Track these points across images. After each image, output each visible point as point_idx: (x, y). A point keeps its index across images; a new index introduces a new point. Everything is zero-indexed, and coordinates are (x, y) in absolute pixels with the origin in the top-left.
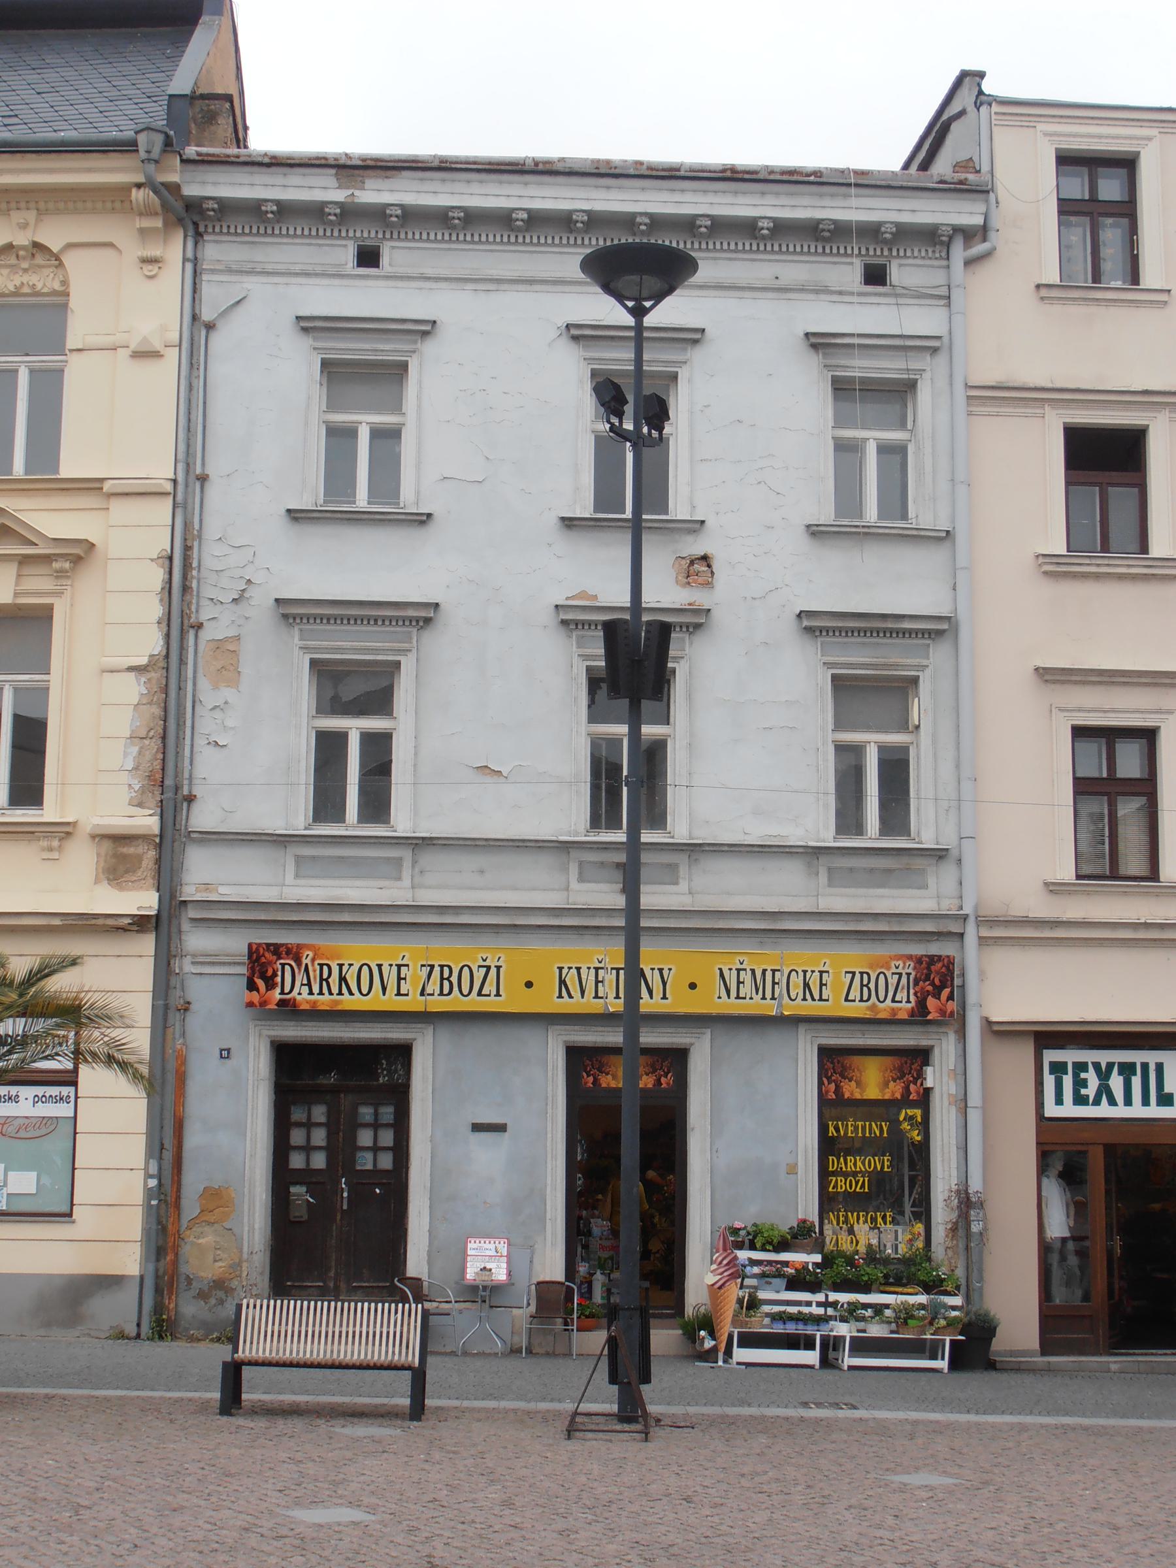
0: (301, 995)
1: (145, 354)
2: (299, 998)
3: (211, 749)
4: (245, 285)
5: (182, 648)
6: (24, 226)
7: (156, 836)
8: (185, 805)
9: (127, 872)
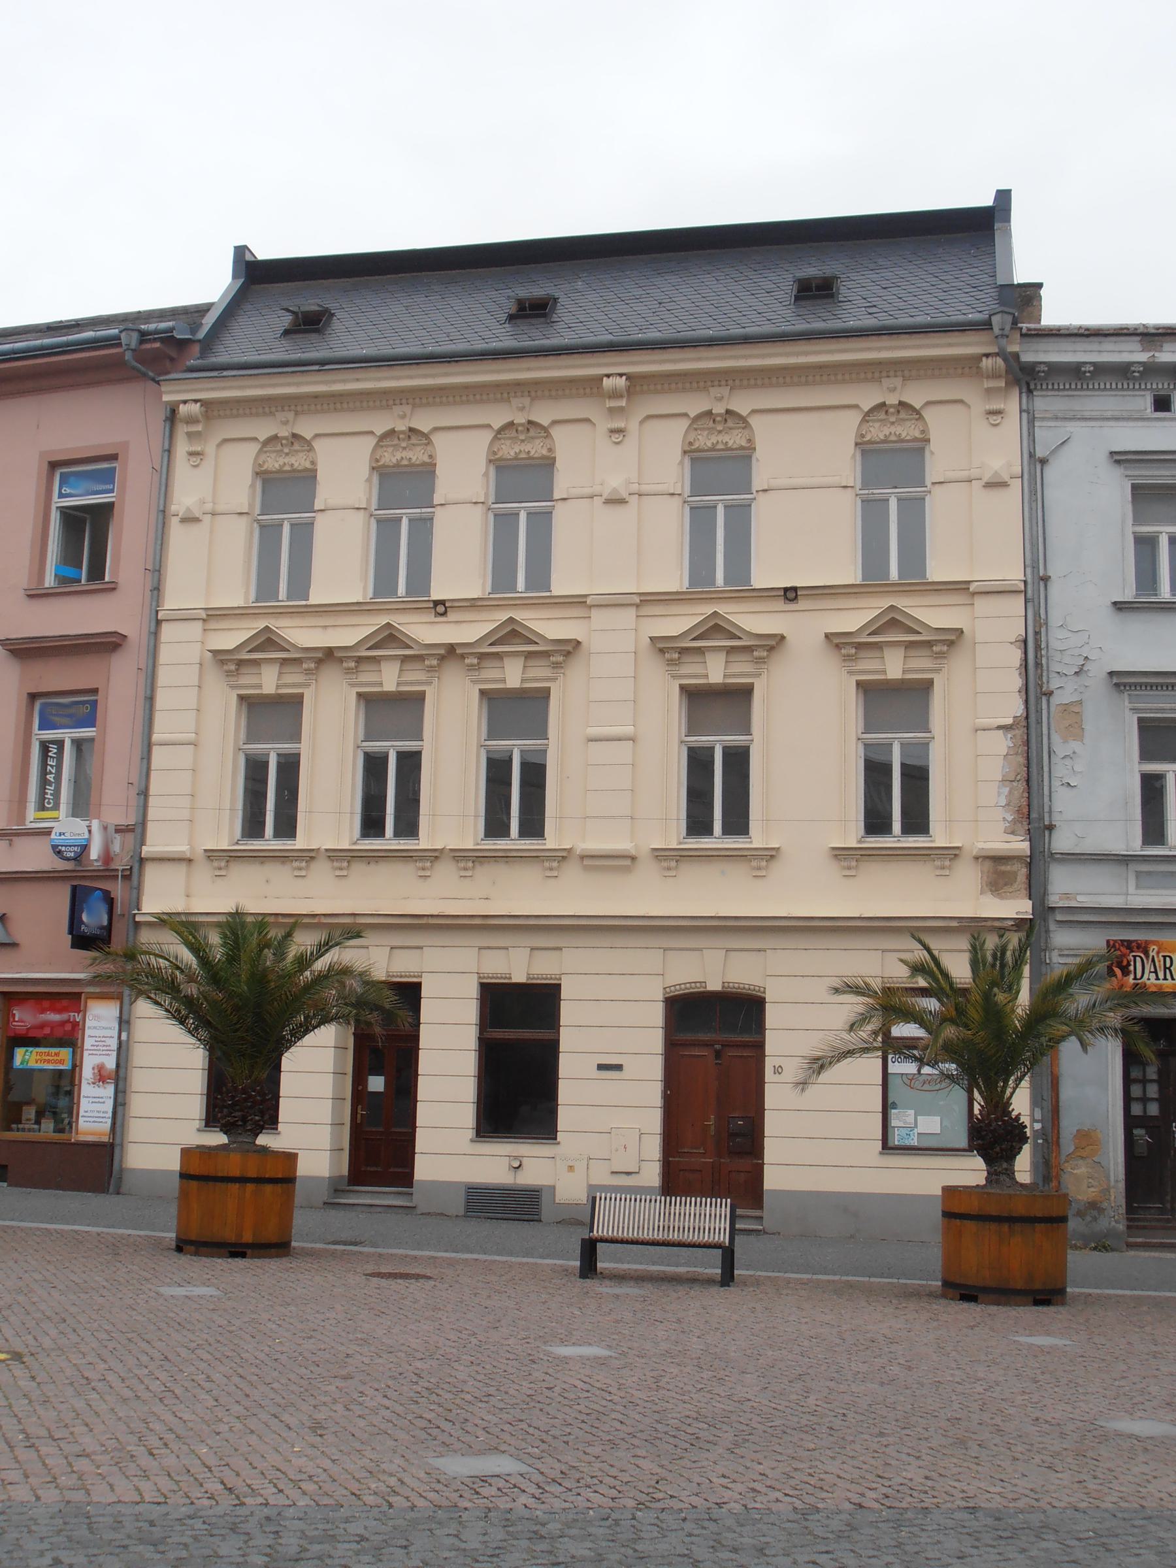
0: (1150, 980)
1: (996, 484)
2: (1148, 982)
3: (1064, 789)
4: (1068, 429)
5: (1039, 712)
7: (1027, 857)
8: (1047, 833)
9: (1006, 885)
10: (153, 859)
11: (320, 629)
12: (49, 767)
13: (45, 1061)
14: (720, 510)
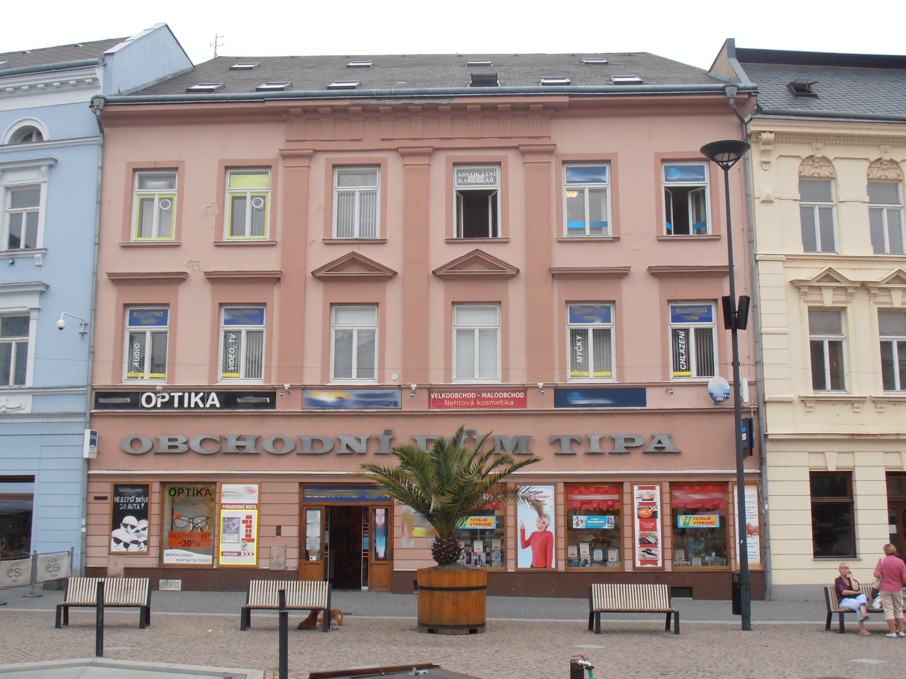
6: (817, 149)
10: (771, 402)
11: (850, 271)
12: (680, 345)
13: (700, 523)
14: (885, 212)
